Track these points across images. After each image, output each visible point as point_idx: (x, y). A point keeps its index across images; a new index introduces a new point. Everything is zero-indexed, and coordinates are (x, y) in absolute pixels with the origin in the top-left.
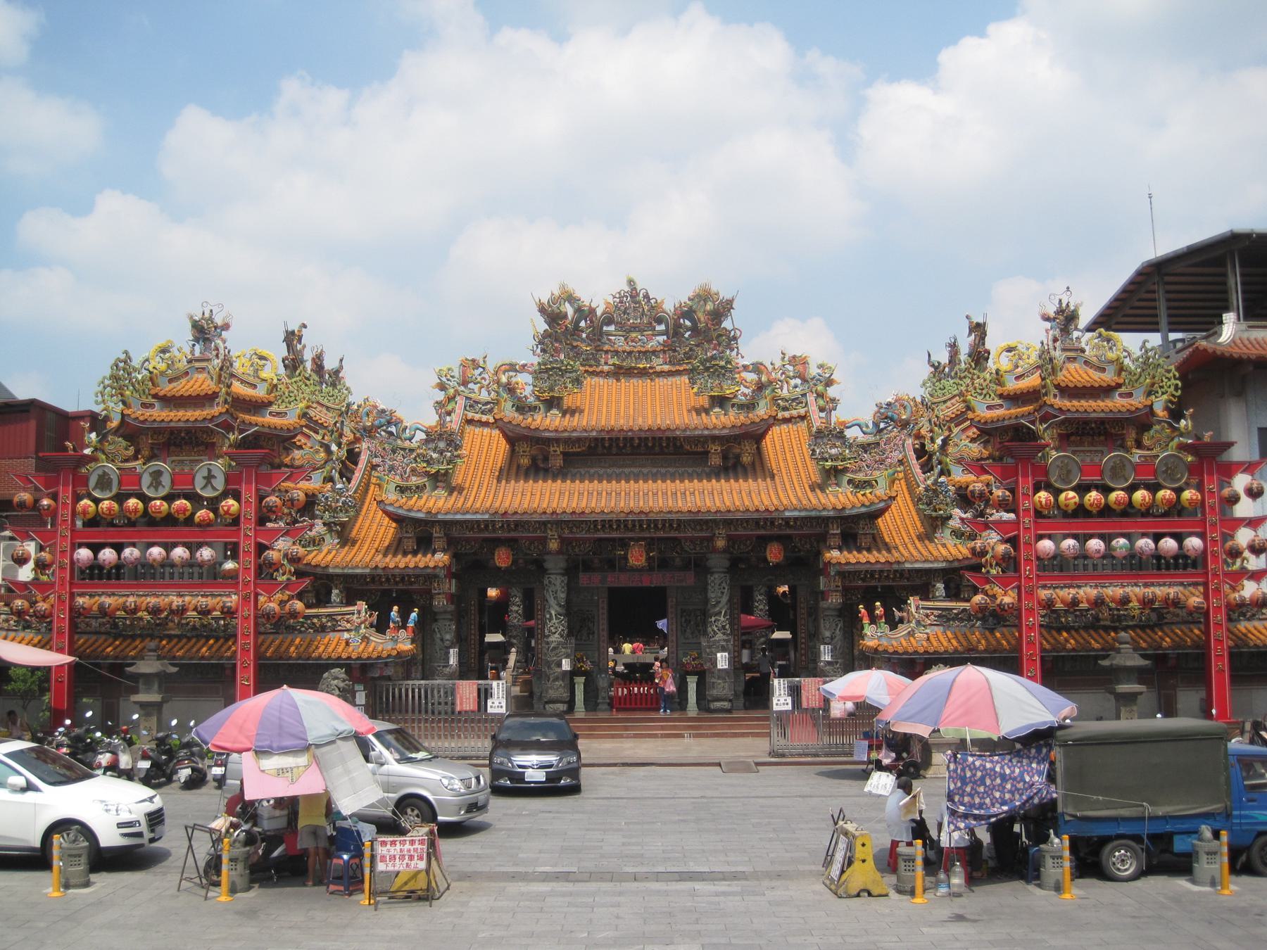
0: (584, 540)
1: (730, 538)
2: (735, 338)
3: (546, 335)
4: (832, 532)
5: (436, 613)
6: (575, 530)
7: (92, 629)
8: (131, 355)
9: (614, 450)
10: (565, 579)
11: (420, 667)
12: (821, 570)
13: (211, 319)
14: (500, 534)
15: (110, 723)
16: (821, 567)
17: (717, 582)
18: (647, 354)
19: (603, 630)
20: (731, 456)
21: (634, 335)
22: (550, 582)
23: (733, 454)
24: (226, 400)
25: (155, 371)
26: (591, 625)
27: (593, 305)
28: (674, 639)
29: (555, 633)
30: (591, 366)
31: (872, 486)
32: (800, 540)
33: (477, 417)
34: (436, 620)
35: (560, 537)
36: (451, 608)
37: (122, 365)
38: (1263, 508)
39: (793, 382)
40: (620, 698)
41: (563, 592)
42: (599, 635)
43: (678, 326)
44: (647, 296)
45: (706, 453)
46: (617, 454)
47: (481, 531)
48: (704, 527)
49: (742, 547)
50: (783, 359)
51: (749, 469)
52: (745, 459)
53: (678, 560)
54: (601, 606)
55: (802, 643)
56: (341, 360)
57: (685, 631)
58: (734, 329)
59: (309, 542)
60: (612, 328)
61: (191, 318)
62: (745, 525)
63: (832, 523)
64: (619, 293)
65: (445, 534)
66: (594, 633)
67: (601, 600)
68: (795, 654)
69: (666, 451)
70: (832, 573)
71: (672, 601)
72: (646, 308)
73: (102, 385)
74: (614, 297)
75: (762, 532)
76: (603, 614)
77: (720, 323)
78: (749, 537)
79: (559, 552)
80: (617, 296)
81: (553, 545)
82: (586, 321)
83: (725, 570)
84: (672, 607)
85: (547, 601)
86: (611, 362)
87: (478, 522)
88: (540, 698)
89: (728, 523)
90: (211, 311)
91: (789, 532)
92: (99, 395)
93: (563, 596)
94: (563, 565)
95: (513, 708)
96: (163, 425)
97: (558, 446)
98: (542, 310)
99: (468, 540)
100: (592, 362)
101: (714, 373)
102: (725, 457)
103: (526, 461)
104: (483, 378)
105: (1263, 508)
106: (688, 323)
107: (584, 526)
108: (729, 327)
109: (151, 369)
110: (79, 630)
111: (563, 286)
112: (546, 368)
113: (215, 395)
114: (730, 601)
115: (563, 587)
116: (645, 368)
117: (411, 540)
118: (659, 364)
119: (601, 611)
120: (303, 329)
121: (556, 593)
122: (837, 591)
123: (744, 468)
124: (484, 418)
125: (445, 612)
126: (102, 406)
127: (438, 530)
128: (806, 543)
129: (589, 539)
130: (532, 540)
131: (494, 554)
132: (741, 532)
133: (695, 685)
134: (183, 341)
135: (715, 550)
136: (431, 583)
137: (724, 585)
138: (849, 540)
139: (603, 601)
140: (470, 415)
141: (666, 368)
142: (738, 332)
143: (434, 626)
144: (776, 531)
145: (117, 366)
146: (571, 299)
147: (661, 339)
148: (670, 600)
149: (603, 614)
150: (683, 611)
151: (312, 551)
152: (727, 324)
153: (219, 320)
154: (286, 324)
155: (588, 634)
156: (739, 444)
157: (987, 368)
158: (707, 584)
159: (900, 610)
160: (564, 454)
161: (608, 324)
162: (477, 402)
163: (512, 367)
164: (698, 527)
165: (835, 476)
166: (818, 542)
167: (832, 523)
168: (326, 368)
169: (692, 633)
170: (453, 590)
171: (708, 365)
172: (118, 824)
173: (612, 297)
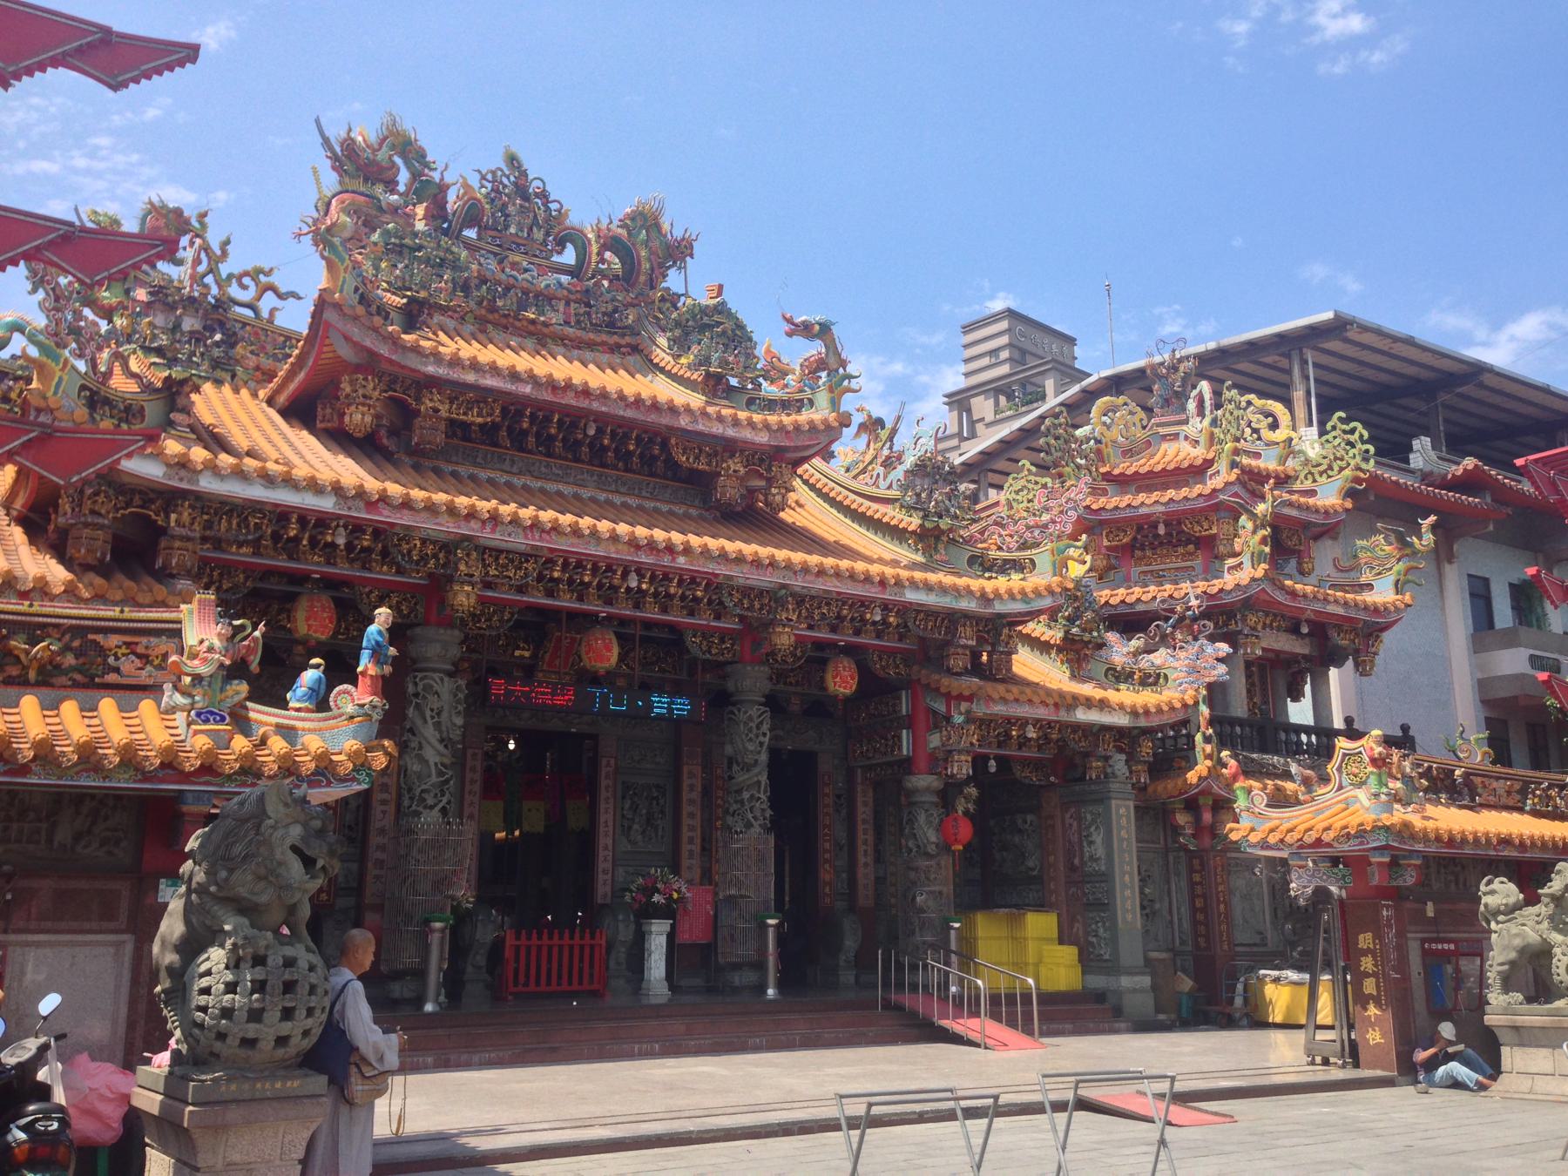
15: (512, 746)
16: (904, 712)
18: (544, 299)
27: (448, 179)
28: (610, 842)
29: (432, 807)
40: (1328, 965)
41: (459, 713)
44: (544, 195)
57: (630, 828)
64: (494, 173)
67: (470, 752)
68: (852, 881)
71: (608, 765)
74: (483, 178)
76: (473, 782)
80: (489, 177)
83: (763, 700)
84: (607, 777)
85: (412, 731)
87: (282, 514)
95: (442, 998)
112: (402, 245)
115: (458, 702)
116: (533, 322)
121: (439, 714)
122: (968, 752)
127: (186, 516)
139: (474, 755)
148: (604, 761)
157: (136, 709)
172: (193, 60)
173: (478, 176)
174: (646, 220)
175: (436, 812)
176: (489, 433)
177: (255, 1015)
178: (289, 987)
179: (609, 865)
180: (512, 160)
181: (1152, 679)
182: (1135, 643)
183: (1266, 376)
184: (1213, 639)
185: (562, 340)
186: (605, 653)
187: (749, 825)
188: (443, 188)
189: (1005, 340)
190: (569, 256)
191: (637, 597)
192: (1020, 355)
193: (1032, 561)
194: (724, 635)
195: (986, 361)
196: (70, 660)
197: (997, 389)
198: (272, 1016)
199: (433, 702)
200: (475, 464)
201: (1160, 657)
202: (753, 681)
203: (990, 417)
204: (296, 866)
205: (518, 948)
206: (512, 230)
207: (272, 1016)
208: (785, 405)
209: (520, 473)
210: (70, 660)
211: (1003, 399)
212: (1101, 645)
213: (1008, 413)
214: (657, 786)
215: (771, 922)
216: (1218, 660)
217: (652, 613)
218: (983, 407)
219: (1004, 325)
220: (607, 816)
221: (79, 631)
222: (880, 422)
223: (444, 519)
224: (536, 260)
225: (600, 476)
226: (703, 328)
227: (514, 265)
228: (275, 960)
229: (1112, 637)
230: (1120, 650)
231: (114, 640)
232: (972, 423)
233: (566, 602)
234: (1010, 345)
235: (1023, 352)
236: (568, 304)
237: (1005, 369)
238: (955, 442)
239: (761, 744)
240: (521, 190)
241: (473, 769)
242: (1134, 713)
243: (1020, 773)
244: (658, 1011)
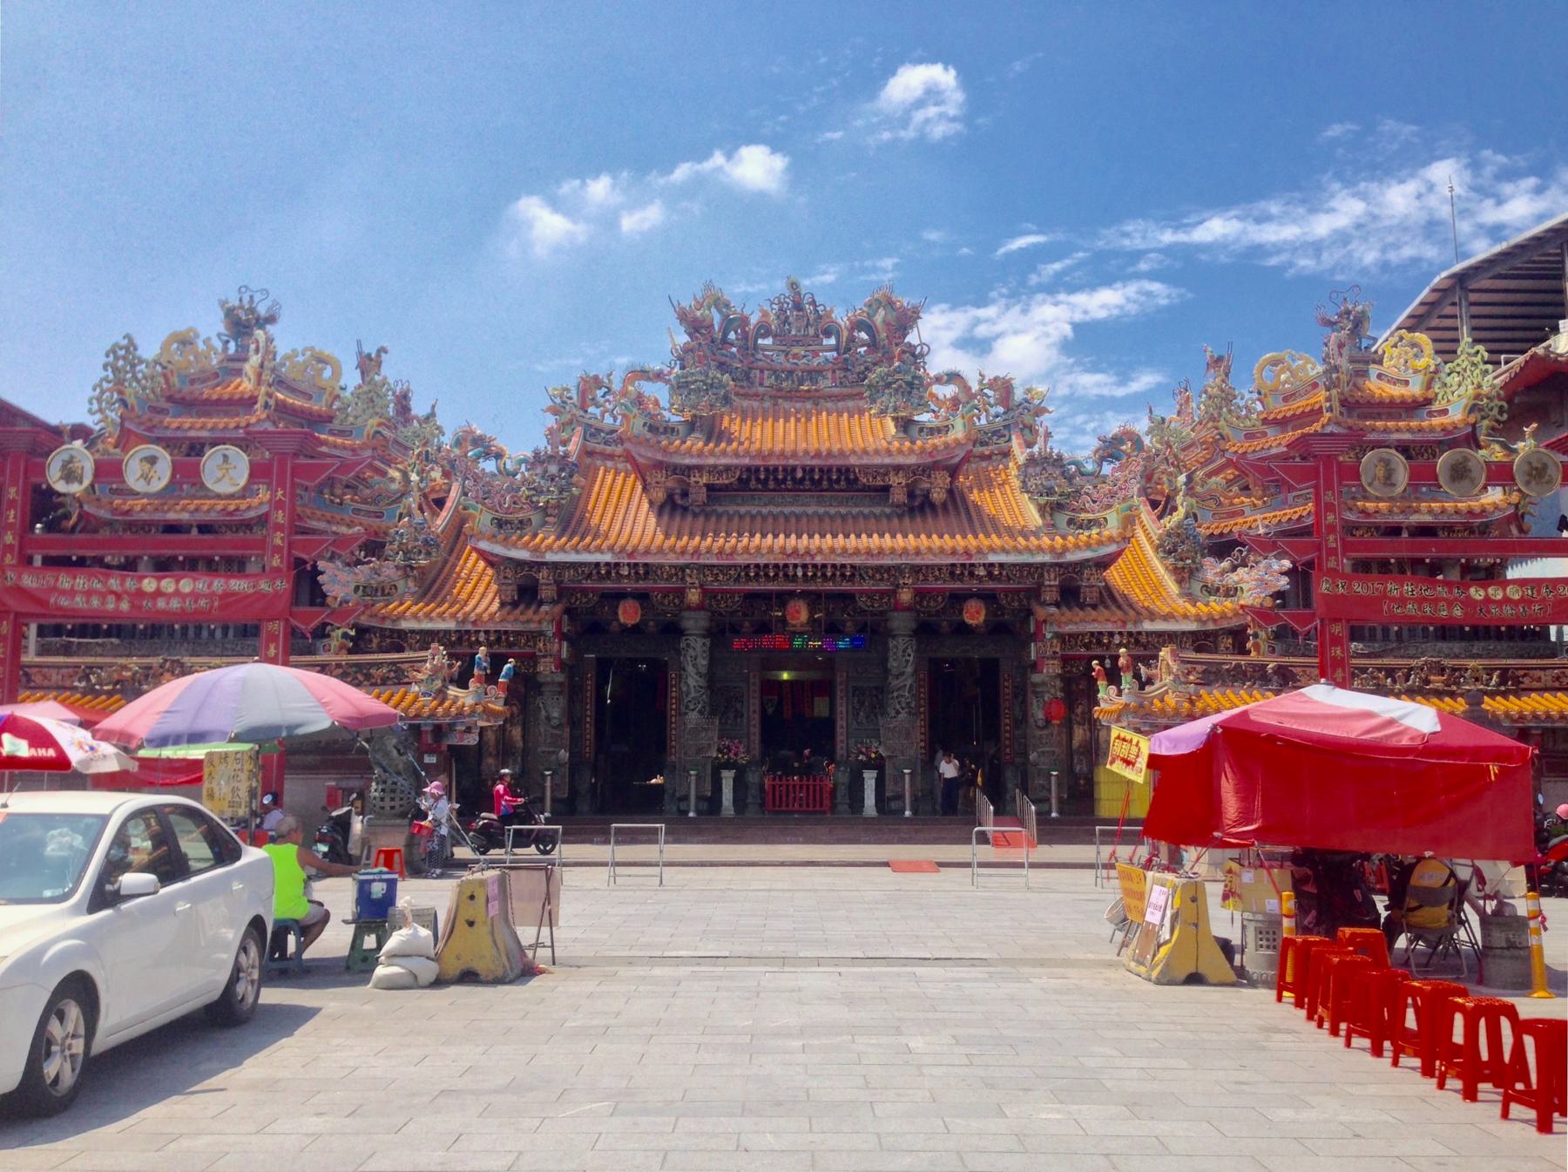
0: (732, 593)
1: (920, 594)
2: (922, 355)
3: (687, 350)
4: (1047, 583)
5: (540, 685)
6: (721, 577)
7: (53, 682)
8: (137, 341)
9: (771, 485)
10: (708, 641)
11: (519, 759)
12: (1032, 635)
13: (252, 310)
14: (628, 585)
17: (901, 647)
18: (814, 374)
19: (754, 712)
20: (918, 492)
21: (796, 350)
22: (688, 645)
23: (922, 490)
24: (266, 403)
25: (170, 366)
26: (739, 706)
27: (747, 312)
30: (742, 387)
31: (1100, 525)
32: (1006, 596)
33: (600, 448)
34: (541, 694)
35: (701, 586)
36: (560, 678)
37: (122, 352)
38: (1098, 853)
39: (993, 411)
42: (748, 717)
43: (852, 339)
45: (886, 489)
46: (774, 490)
47: (601, 578)
48: (885, 575)
49: (932, 604)
50: (981, 382)
51: (940, 511)
52: (935, 495)
53: (849, 624)
54: (752, 680)
55: (1006, 731)
56: (433, 407)
58: (922, 344)
59: (377, 590)
60: (769, 341)
61: (223, 303)
62: (937, 573)
63: (1048, 571)
64: (779, 298)
65: (555, 581)
66: (742, 716)
69: (836, 487)
70: (1049, 636)
72: (812, 317)
73: (98, 390)
74: (772, 303)
75: (958, 585)
77: (905, 336)
78: (940, 591)
79: (700, 607)
81: (693, 596)
82: (736, 332)
86: (767, 383)
88: (673, 795)
89: (916, 570)
90: (251, 297)
91: (991, 585)
92: (95, 401)
93: (705, 662)
94: (704, 623)
96: (179, 434)
97: (701, 477)
98: (683, 317)
99: (584, 591)
100: (745, 384)
101: (896, 390)
102: (911, 495)
103: (660, 495)
104: (608, 401)
105: (1098, 853)
106: (864, 335)
107: (732, 572)
108: (915, 342)
109: (165, 364)
110: (32, 684)
111: (708, 286)
113: (253, 400)
114: (916, 671)
116: (809, 391)
117: (510, 588)
118: (825, 384)
119: (752, 688)
120: (383, 355)
122: (1054, 658)
123: (932, 506)
124: (609, 449)
125: (553, 683)
126: (98, 416)
128: (1013, 600)
129: (739, 592)
130: (666, 592)
131: (617, 614)
132: (933, 585)
133: (873, 782)
134: (211, 328)
135: (898, 607)
136: (535, 644)
137: (909, 651)
138: (1070, 595)
140: (591, 445)
141: (836, 390)
142: (926, 349)
143: (539, 701)
144: (974, 585)
145: (114, 352)
146: (721, 304)
147: (832, 355)
149: (754, 712)
150: (855, 689)
151: (379, 601)
152: (912, 338)
153: (262, 310)
154: (359, 343)
155: (736, 717)
156: (929, 476)
158: (887, 650)
159: (1148, 666)
160: (710, 488)
161: (764, 336)
162: (599, 430)
163: (644, 374)
164: (878, 576)
165: (1051, 515)
166: (1029, 599)
167: (1048, 571)
168: (413, 412)
169: (867, 717)
170: (564, 655)
171: (890, 379)
175: (695, 713)
176: (743, 484)
177: (382, 799)
178: (393, 791)
179: (844, 738)
182: (1225, 564)
183: (1512, 287)
185: (830, 397)
187: (898, 713)
193: (1105, 519)
196: (392, 674)
198: (387, 799)
199: (691, 652)
200: (738, 505)
204: (395, 753)
205: (774, 787)
206: (793, 333)
207: (387, 799)
208: (933, 431)
209: (765, 505)
210: (392, 674)
214: (876, 688)
215: (906, 771)
216: (1282, 574)
220: (842, 708)
221: (394, 664)
223: (671, 556)
224: (810, 348)
225: (818, 497)
226: (888, 385)
227: (795, 356)
228: (389, 782)
230: (1212, 570)
231: (406, 665)
236: (834, 372)
239: (907, 661)
241: (754, 684)
244: (869, 821)
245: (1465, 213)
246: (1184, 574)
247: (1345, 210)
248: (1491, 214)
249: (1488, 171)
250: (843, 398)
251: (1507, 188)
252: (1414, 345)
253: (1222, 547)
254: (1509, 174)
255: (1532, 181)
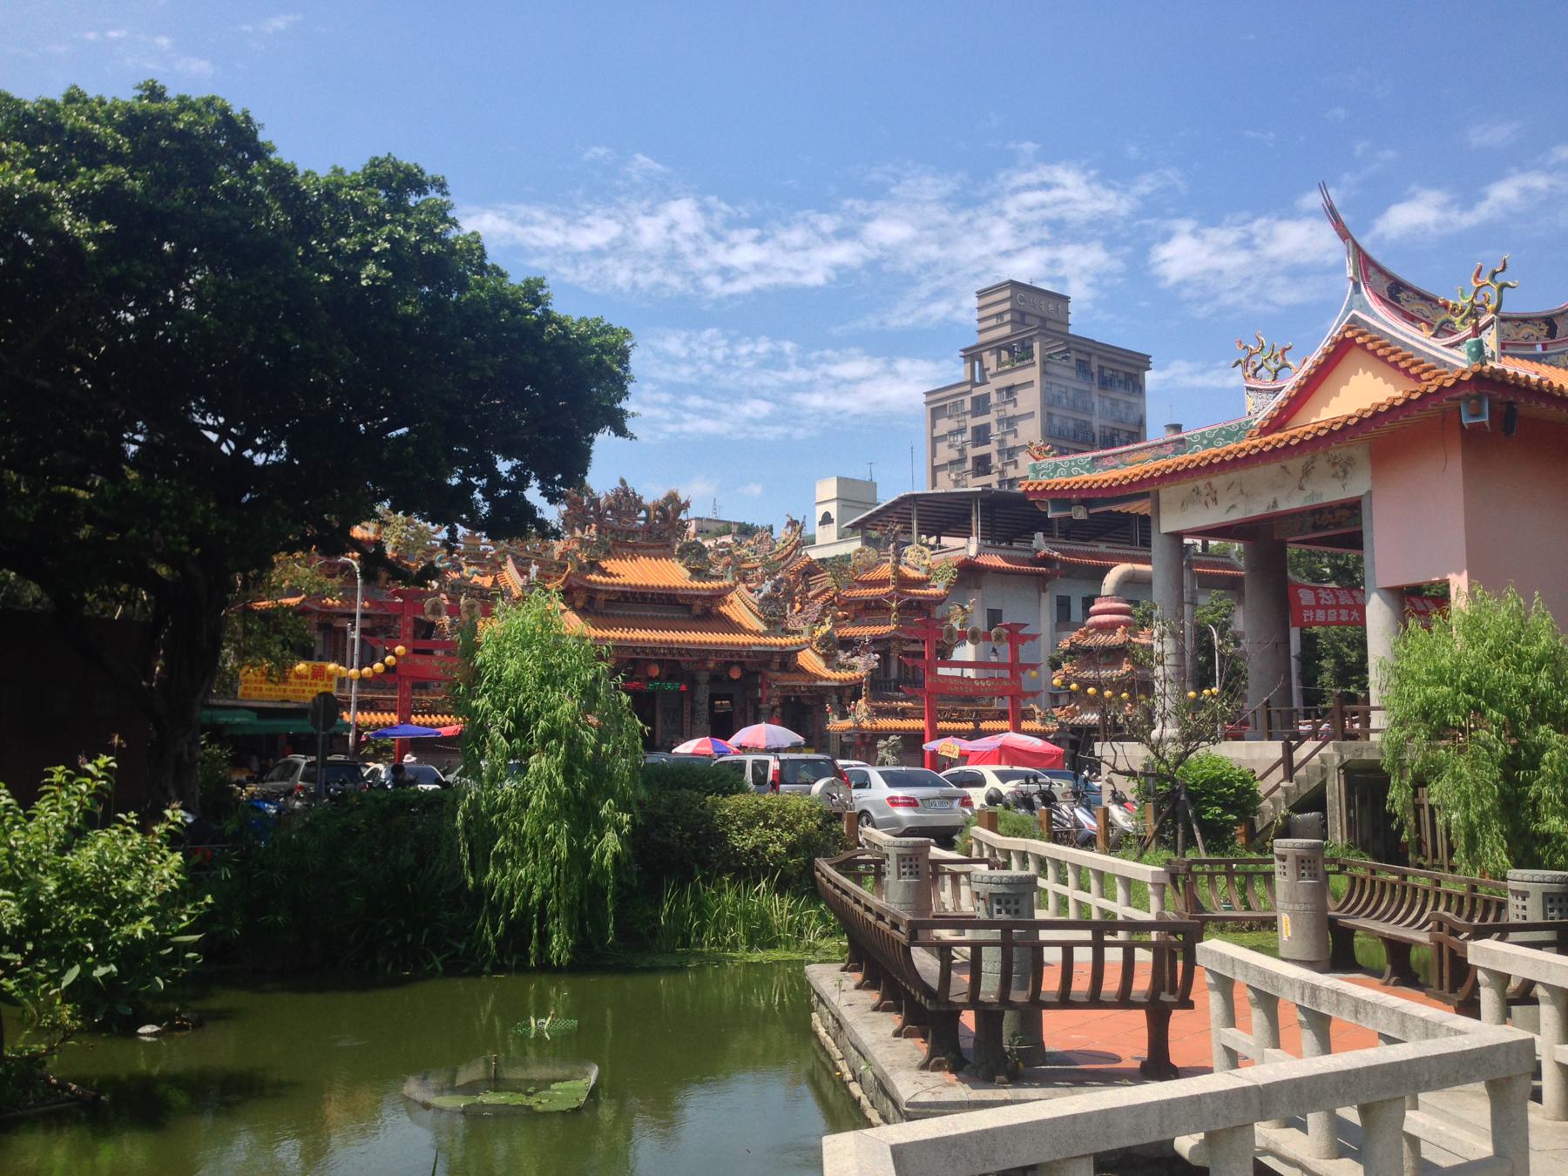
18: (634, 533)
174: (672, 497)
176: (618, 600)
180: (623, 482)
181: (852, 668)
184: (874, 653)
185: (642, 547)
186: (655, 671)
188: (599, 499)
189: (1007, 306)
190: (643, 514)
191: (665, 654)
192: (1020, 317)
194: (694, 662)
195: (993, 322)
197: (997, 346)
201: (855, 660)
202: (703, 677)
203: (993, 369)
211: (1005, 355)
212: (837, 655)
213: (1007, 367)
217: (670, 657)
218: (990, 360)
219: (1007, 293)
222: (797, 522)
226: (690, 550)
229: (840, 652)
230: (842, 656)
232: (983, 371)
233: (642, 656)
234: (1011, 310)
235: (1023, 314)
237: (1006, 330)
238: (968, 388)
240: (626, 494)
242: (840, 680)
243: (806, 702)
245: (700, 252)
246: (829, 659)
247: (598, 232)
248: (720, 254)
249: (718, 217)
250: (648, 547)
251: (735, 236)
252: (921, 552)
253: (848, 644)
254: (734, 223)
255: (755, 232)
